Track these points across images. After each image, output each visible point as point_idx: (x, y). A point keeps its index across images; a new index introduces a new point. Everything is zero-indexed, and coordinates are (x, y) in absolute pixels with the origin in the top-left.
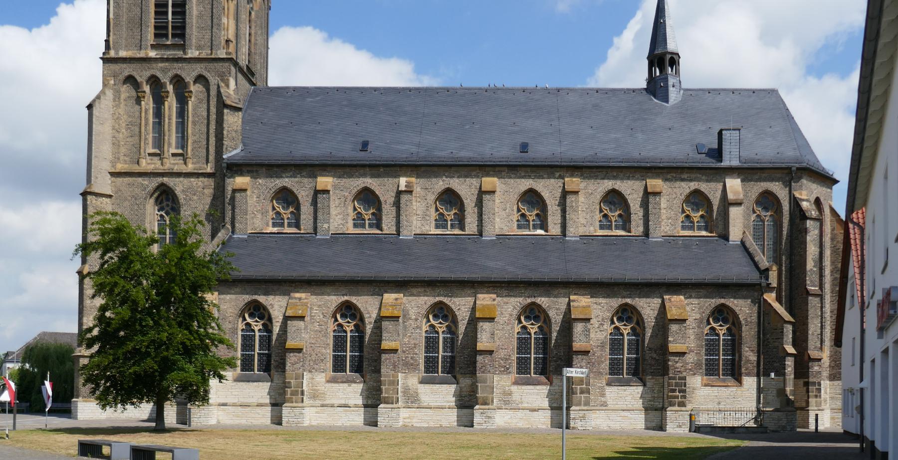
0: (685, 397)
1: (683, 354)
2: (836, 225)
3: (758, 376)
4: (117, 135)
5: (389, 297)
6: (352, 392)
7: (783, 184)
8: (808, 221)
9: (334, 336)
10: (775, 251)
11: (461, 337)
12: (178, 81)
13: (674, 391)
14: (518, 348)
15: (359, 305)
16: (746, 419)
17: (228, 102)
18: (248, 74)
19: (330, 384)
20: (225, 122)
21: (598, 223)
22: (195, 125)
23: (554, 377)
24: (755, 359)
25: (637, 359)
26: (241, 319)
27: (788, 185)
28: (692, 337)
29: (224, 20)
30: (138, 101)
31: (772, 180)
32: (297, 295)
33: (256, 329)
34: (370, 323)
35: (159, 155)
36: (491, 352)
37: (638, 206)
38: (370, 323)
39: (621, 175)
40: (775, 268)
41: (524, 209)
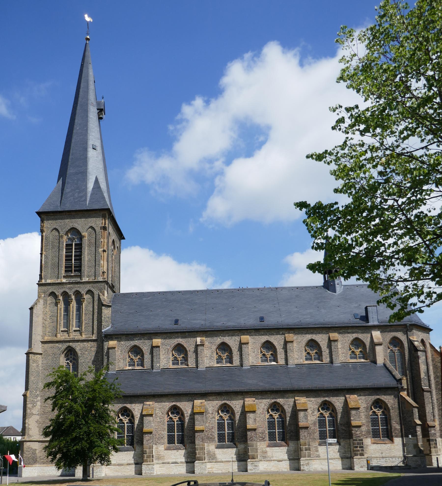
0: (363, 450)
1: (359, 427)
2: (434, 353)
3: (402, 437)
4: (45, 322)
5: (197, 402)
6: (179, 455)
7: (403, 333)
8: (419, 352)
9: (168, 424)
10: (402, 368)
11: (237, 422)
12: (78, 294)
13: (357, 447)
14: (268, 427)
15: (181, 407)
16: (398, 462)
17: (105, 303)
18: (112, 287)
19: (167, 451)
20: (103, 313)
21: (305, 357)
22: (86, 315)
23: (290, 442)
24: (399, 427)
25: (334, 430)
26: (117, 417)
27: (406, 333)
28: (363, 417)
29: (102, 262)
30: (56, 304)
31: (397, 331)
32: (148, 403)
33: (125, 422)
34: (187, 416)
35: (67, 331)
36: (255, 430)
37: (326, 347)
38: (187, 416)
39: (316, 332)
40: (405, 378)
41: (264, 351)
